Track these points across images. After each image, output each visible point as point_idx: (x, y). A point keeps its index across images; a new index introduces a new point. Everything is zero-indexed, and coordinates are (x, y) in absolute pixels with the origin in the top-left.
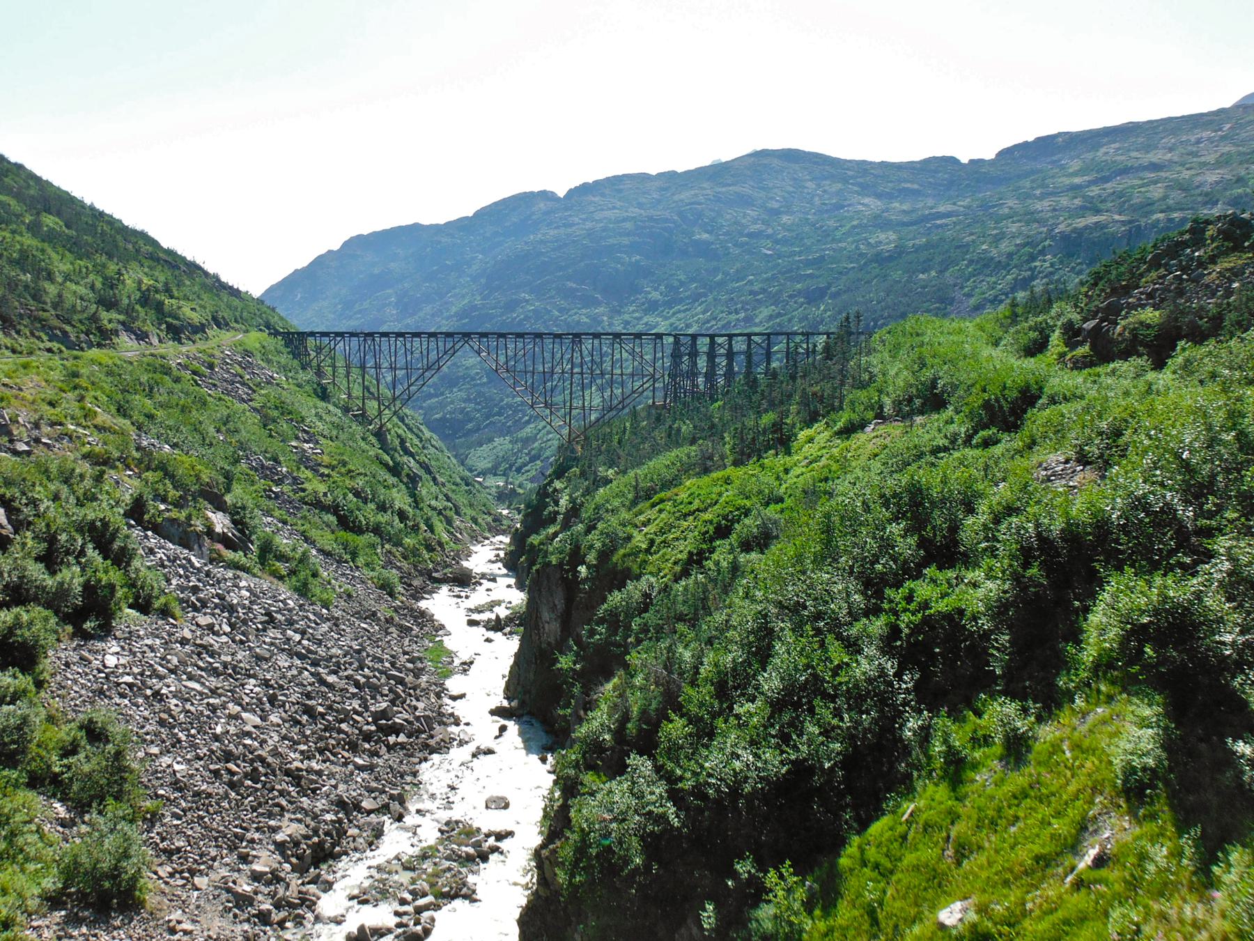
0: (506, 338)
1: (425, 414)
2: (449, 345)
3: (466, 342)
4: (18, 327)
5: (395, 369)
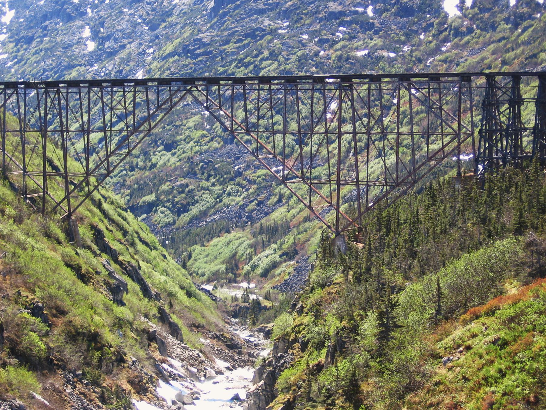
0: (102, 88)
1: (131, 195)
2: (165, 96)
3: (190, 92)
4: (354, 47)
5: (89, 133)
